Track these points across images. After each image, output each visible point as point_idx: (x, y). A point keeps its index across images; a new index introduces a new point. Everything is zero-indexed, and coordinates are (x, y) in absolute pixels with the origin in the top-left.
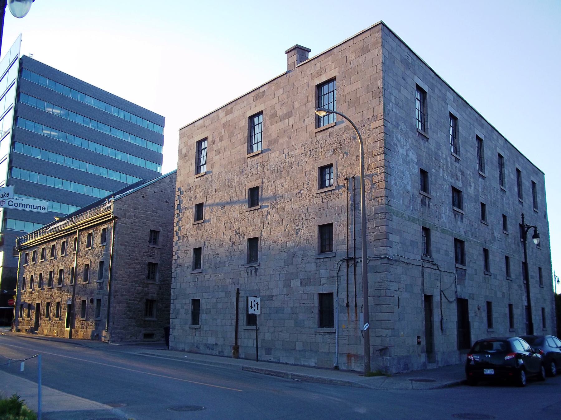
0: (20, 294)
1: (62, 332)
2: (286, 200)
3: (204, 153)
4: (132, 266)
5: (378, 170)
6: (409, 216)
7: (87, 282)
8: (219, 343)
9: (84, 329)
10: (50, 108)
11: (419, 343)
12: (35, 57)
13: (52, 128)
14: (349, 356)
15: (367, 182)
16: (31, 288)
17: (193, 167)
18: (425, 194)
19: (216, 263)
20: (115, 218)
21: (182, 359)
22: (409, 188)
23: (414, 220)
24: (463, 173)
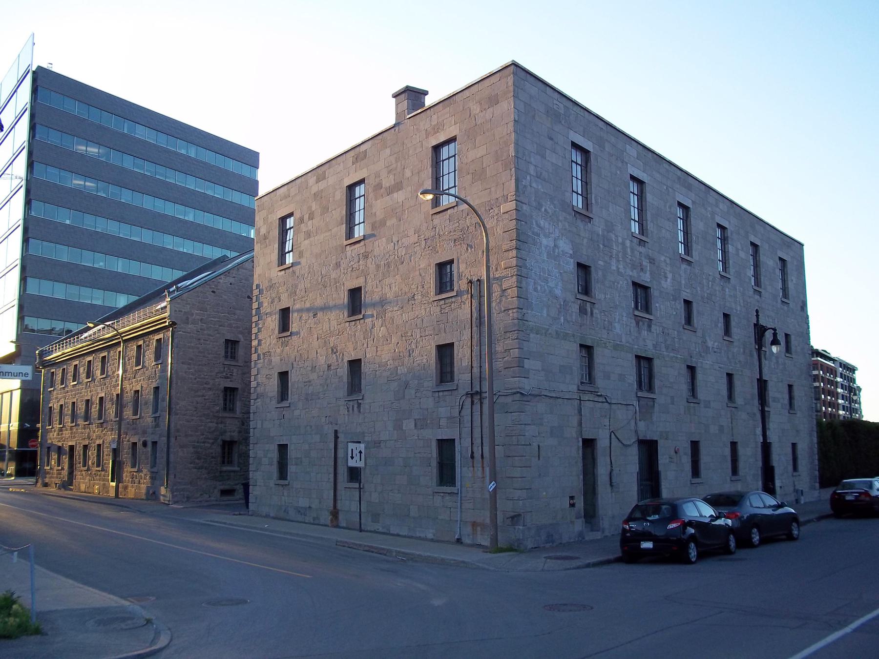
0: (46, 432)
1: (105, 487)
2: (396, 309)
3: (290, 234)
4: (200, 393)
5: (509, 272)
6: (557, 332)
7: (138, 417)
8: (313, 506)
9: (136, 484)
10: (83, 145)
11: (572, 505)
12: (56, 69)
13: (86, 176)
14: (474, 525)
15: (496, 288)
16: (60, 424)
17: (275, 256)
18: (585, 298)
19: (307, 394)
20: (173, 324)
21: (261, 529)
22: (558, 292)
23: (565, 337)
24: (652, 261)
